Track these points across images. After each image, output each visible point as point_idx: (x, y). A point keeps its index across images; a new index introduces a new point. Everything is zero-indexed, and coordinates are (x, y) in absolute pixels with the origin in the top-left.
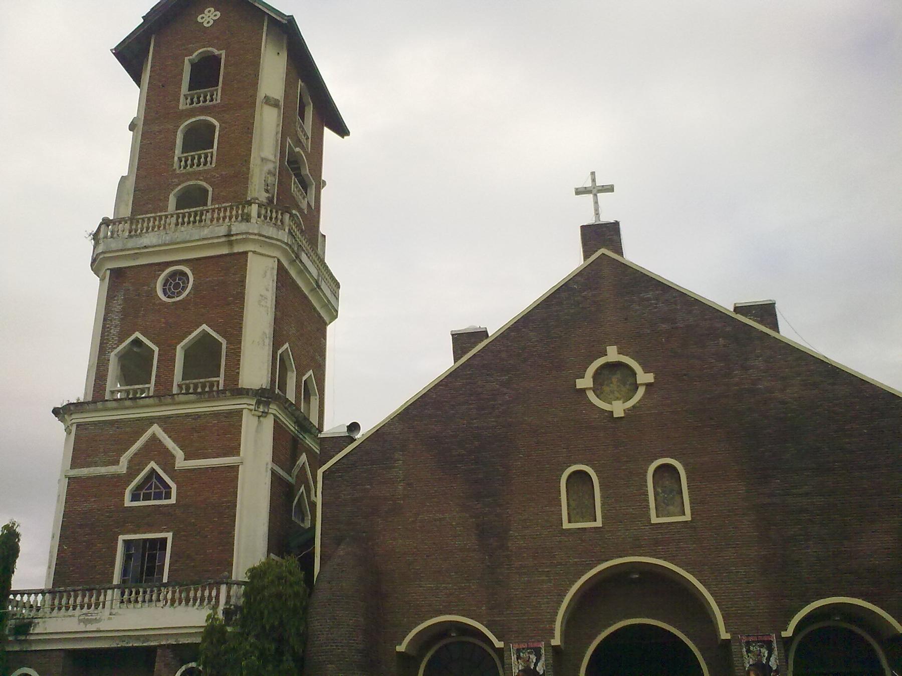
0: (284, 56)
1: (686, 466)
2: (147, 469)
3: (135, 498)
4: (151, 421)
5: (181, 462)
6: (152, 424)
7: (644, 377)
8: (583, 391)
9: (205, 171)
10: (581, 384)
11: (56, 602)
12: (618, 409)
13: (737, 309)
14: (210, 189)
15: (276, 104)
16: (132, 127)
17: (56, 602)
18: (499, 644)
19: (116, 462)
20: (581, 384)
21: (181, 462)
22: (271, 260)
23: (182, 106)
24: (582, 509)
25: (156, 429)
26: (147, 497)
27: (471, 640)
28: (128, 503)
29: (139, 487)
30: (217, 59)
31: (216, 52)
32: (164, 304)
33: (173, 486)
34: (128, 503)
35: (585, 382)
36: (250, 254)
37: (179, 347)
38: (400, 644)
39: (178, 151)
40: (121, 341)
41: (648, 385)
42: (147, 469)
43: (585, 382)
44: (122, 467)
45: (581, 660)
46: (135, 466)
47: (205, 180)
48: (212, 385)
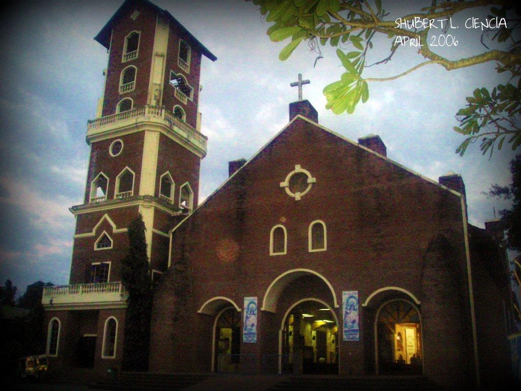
0: (168, 30)
1: (326, 224)
2: (102, 234)
3: (99, 247)
4: (104, 212)
5: (115, 230)
6: (104, 213)
7: (311, 180)
8: (283, 188)
9: (131, 92)
10: (283, 184)
11: (71, 290)
12: (298, 196)
13: (361, 141)
14: (132, 101)
15: (162, 56)
16: (201, 89)
17: (71, 290)
18: (418, 302)
19: (91, 231)
20: (283, 184)
21: (115, 230)
22: (157, 133)
23: (123, 61)
24: (279, 247)
25: (106, 216)
26: (103, 246)
27: (409, 302)
28: (96, 249)
29: (100, 242)
30: (137, 35)
31: (137, 32)
32: (112, 158)
33: (112, 241)
34: (96, 249)
35: (285, 184)
36: (146, 132)
37: (117, 178)
38: (199, 309)
39: (121, 84)
40: (95, 176)
41: (313, 184)
42: (102, 234)
43: (285, 184)
44: (93, 234)
45: (282, 318)
46: (99, 232)
47: (131, 97)
48: (129, 194)
